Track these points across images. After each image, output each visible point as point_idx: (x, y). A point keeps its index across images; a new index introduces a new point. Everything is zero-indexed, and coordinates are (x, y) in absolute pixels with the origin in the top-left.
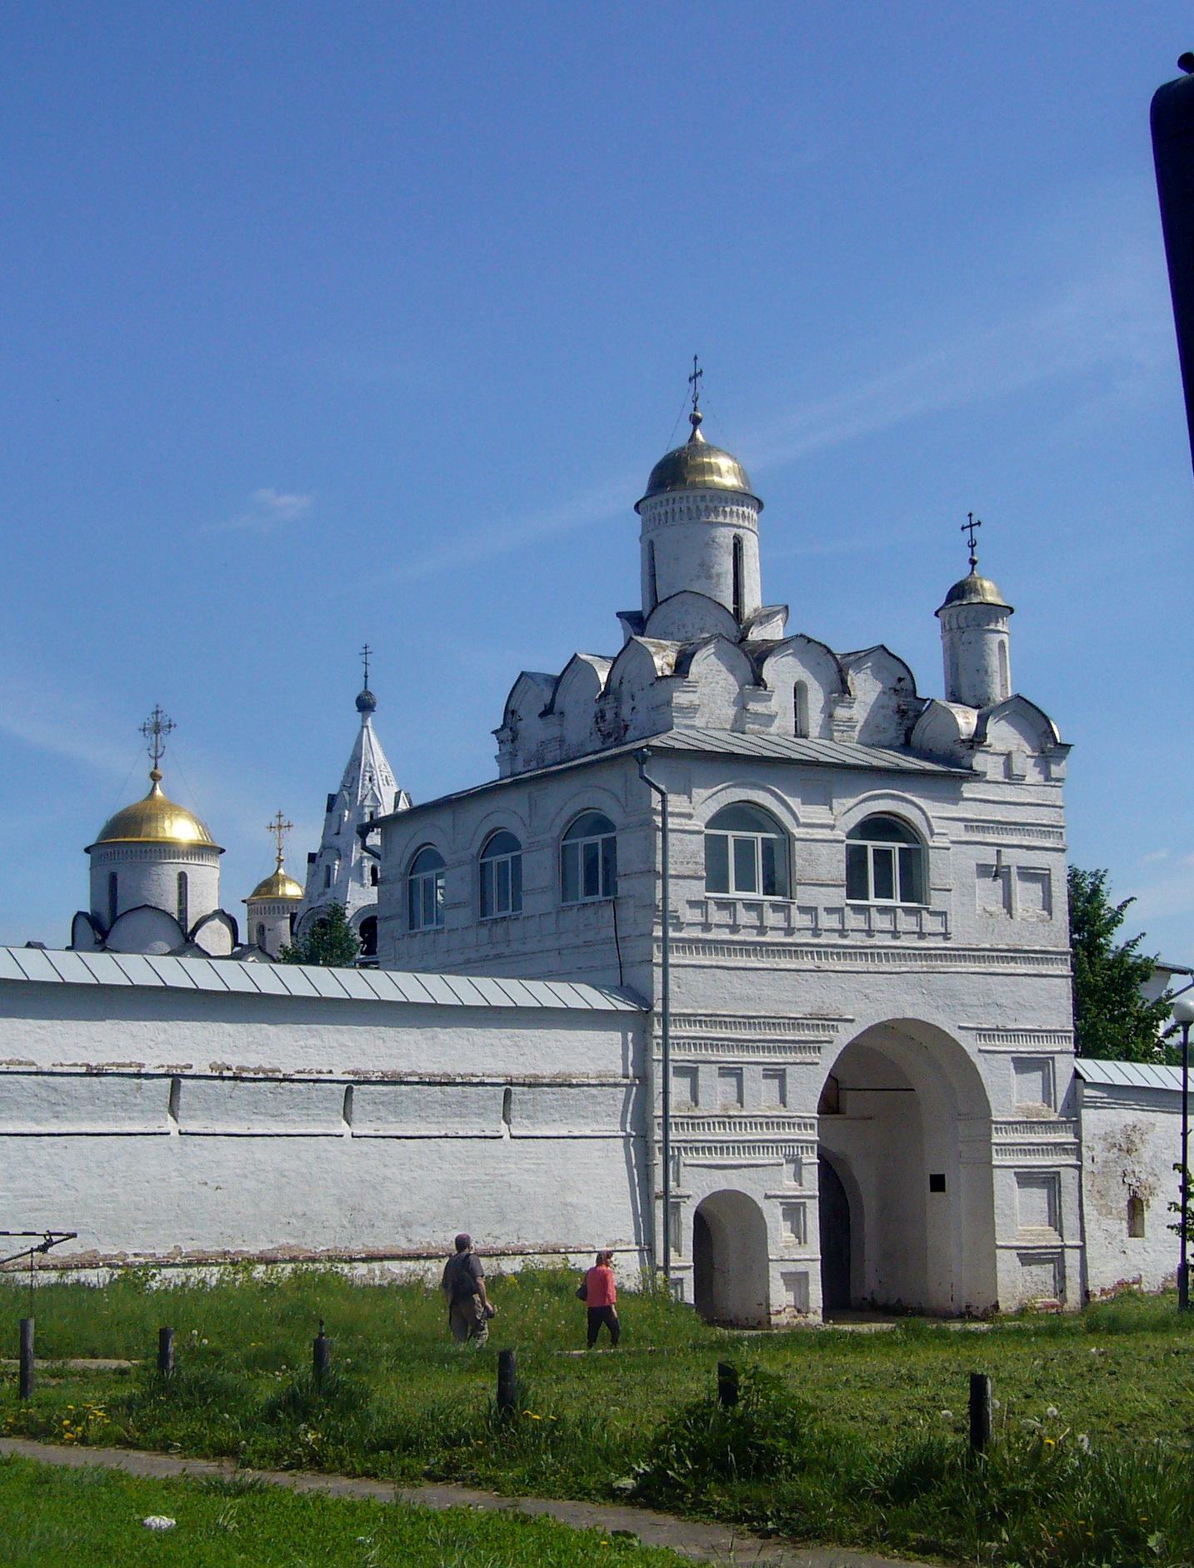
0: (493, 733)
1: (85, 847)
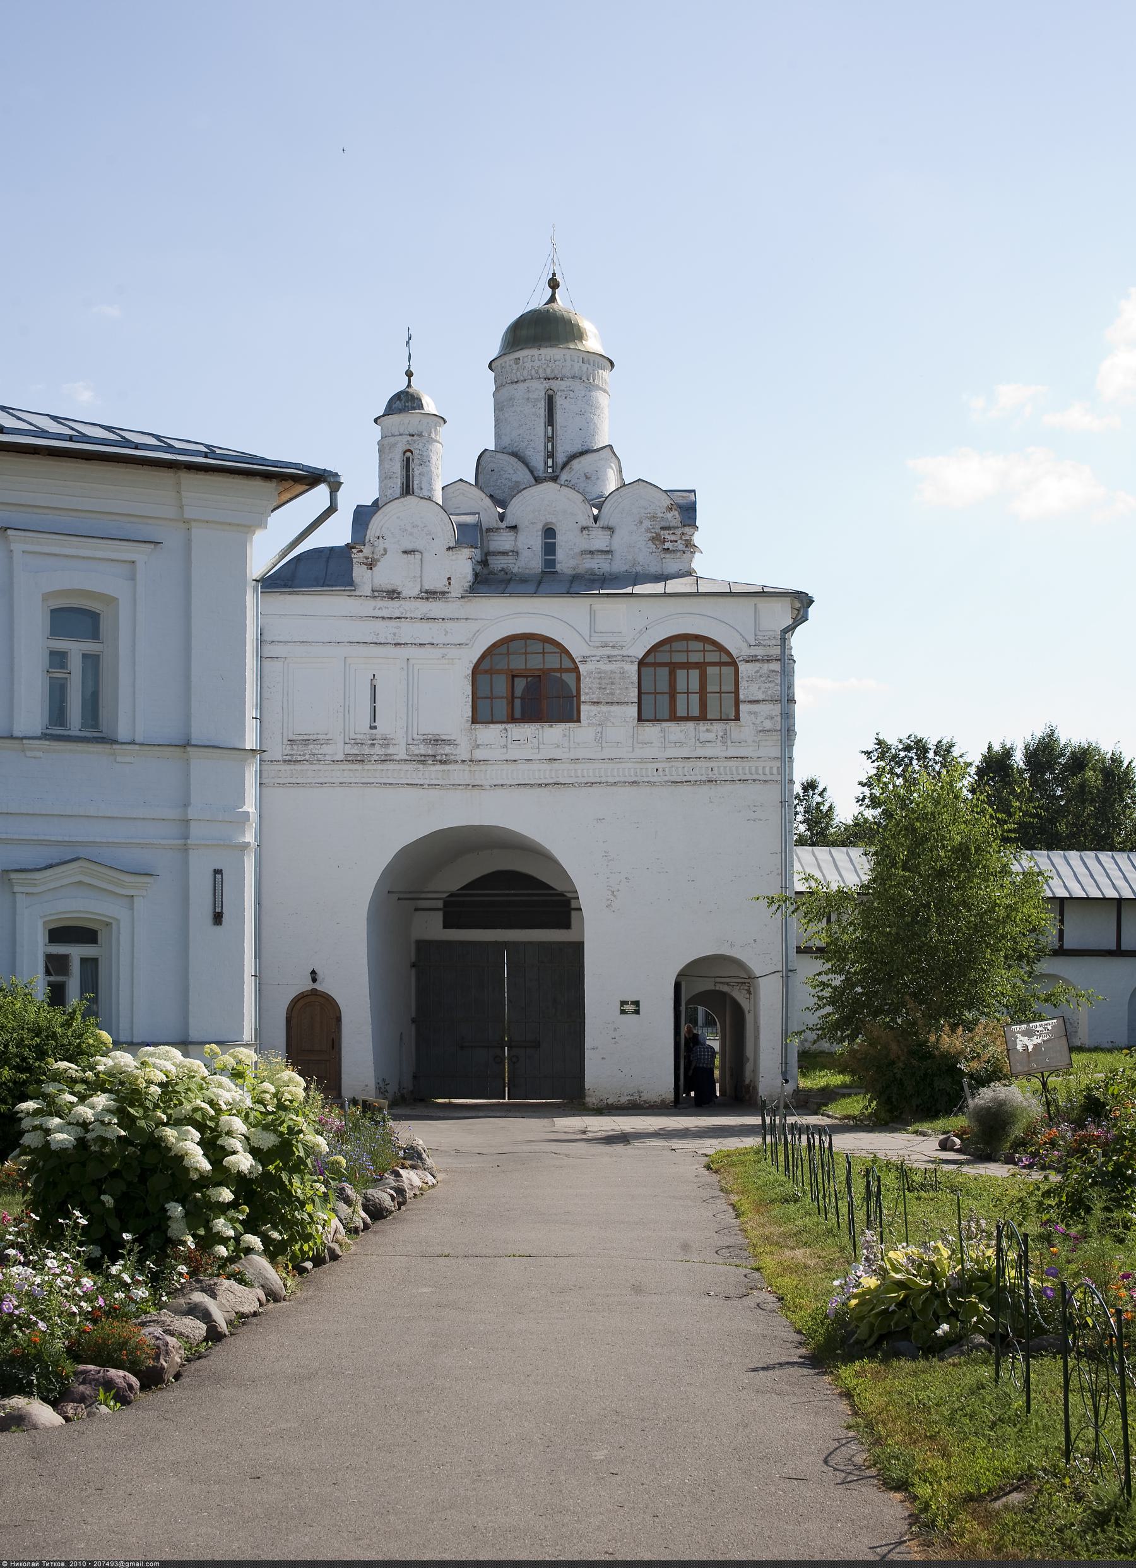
1: (617, 532)
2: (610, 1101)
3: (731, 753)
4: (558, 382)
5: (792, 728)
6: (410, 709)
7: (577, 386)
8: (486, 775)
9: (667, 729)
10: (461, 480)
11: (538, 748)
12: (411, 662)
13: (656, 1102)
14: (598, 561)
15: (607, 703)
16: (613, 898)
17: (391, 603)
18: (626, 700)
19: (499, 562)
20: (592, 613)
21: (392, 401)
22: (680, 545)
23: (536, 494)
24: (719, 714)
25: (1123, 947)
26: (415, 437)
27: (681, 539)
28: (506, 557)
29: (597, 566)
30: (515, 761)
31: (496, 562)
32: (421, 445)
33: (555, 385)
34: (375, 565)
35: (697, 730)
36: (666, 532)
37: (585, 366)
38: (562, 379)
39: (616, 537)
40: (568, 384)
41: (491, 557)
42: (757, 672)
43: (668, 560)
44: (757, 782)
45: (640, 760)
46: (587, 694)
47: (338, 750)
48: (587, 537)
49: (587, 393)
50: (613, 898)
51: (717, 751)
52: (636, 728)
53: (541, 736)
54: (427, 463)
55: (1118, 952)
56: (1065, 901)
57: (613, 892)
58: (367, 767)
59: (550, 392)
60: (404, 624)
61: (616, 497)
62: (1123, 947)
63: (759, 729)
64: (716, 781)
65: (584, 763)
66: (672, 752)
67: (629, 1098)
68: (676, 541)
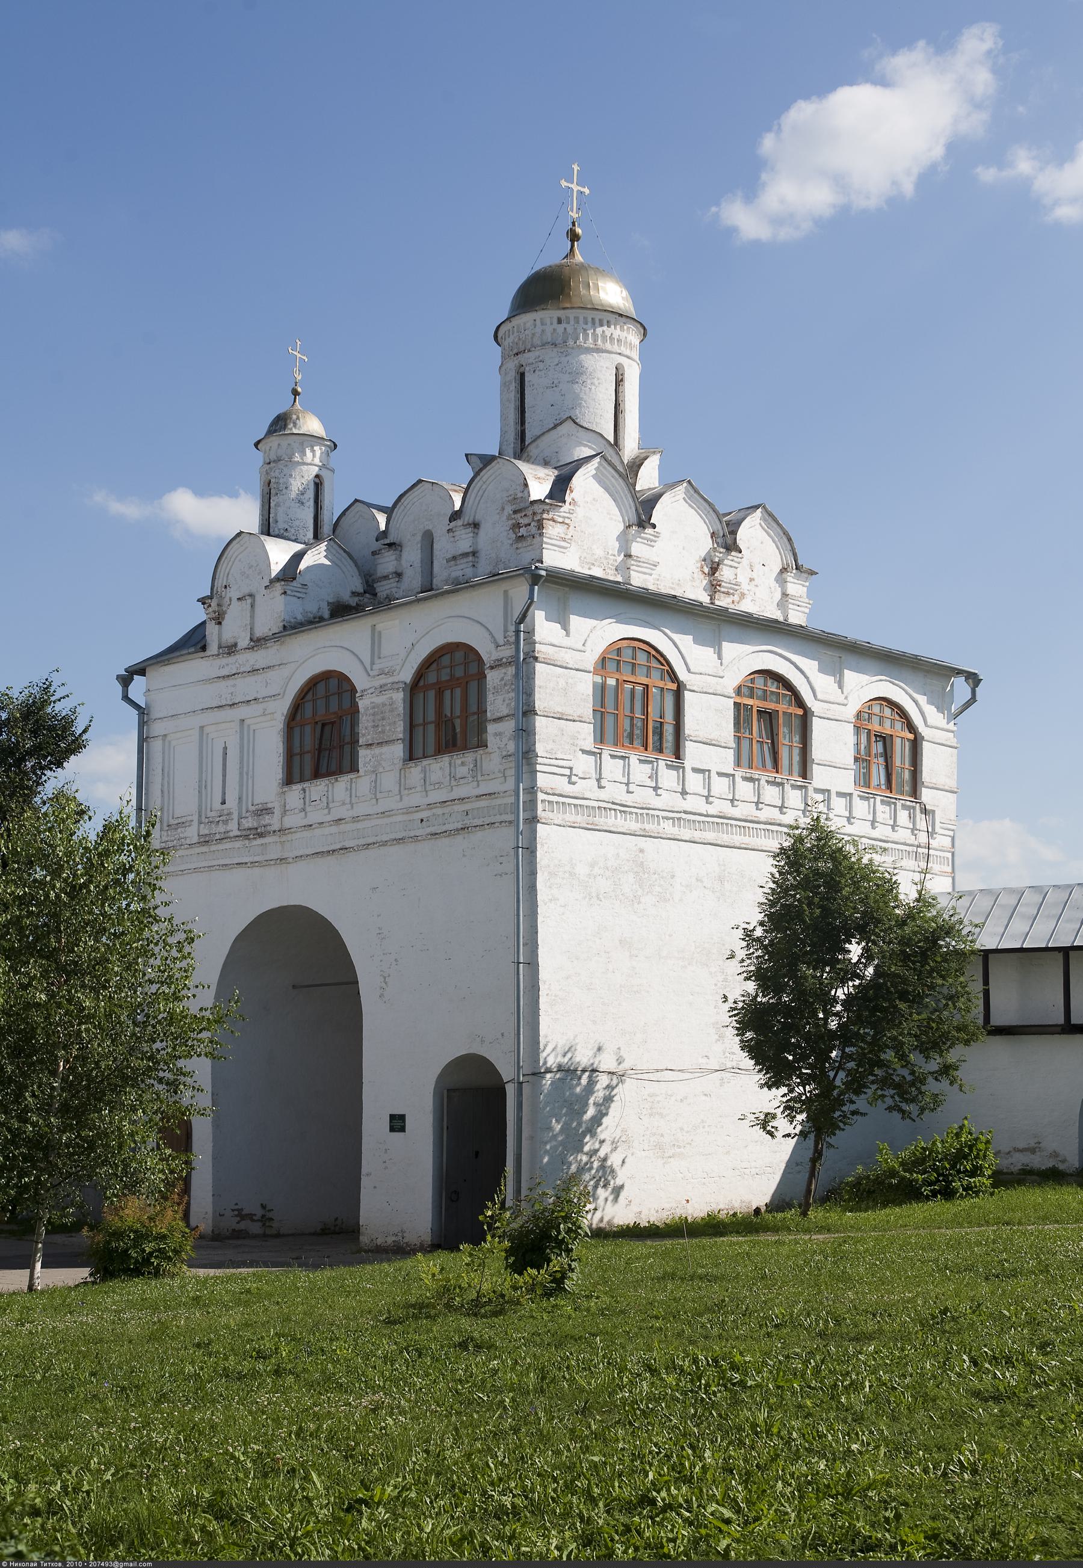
0: (198, 601)
1: (482, 526)
2: (379, 1242)
3: (483, 790)
4: (527, 355)
5: (533, 748)
6: (245, 776)
7: (551, 356)
8: (301, 842)
9: (427, 767)
10: (356, 501)
11: (327, 807)
12: (247, 722)
13: (415, 1245)
14: (462, 567)
15: (378, 744)
16: (385, 986)
17: (231, 659)
18: (394, 737)
19: (387, 587)
20: (374, 632)
21: (271, 425)
22: (533, 529)
23: (415, 500)
24: (702, 735)
25: (1074, 1020)
26: (272, 465)
27: (533, 520)
28: (389, 582)
29: (460, 573)
30: (311, 826)
31: (381, 589)
32: (277, 474)
33: (524, 358)
34: (223, 619)
35: (453, 765)
36: (519, 515)
37: (560, 329)
38: (529, 351)
39: (482, 532)
40: (537, 353)
41: (379, 584)
42: (502, 679)
43: (521, 550)
44: (503, 824)
45: (405, 810)
46: (364, 735)
47: (192, 833)
48: (452, 539)
49: (564, 359)
50: (385, 986)
51: (466, 790)
52: (403, 772)
53: (330, 793)
54: (284, 491)
55: (1069, 1028)
56: (1071, 953)
57: (385, 978)
58: (213, 848)
59: (522, 370)
60: (239, 681)
61: (479, 485)
62: (1074, 1020)
63: (504, 753)
64: (468, 828)
65: (364, 820)
66: (436, 796)
67: (394, 1238)
68: (529, 525)
